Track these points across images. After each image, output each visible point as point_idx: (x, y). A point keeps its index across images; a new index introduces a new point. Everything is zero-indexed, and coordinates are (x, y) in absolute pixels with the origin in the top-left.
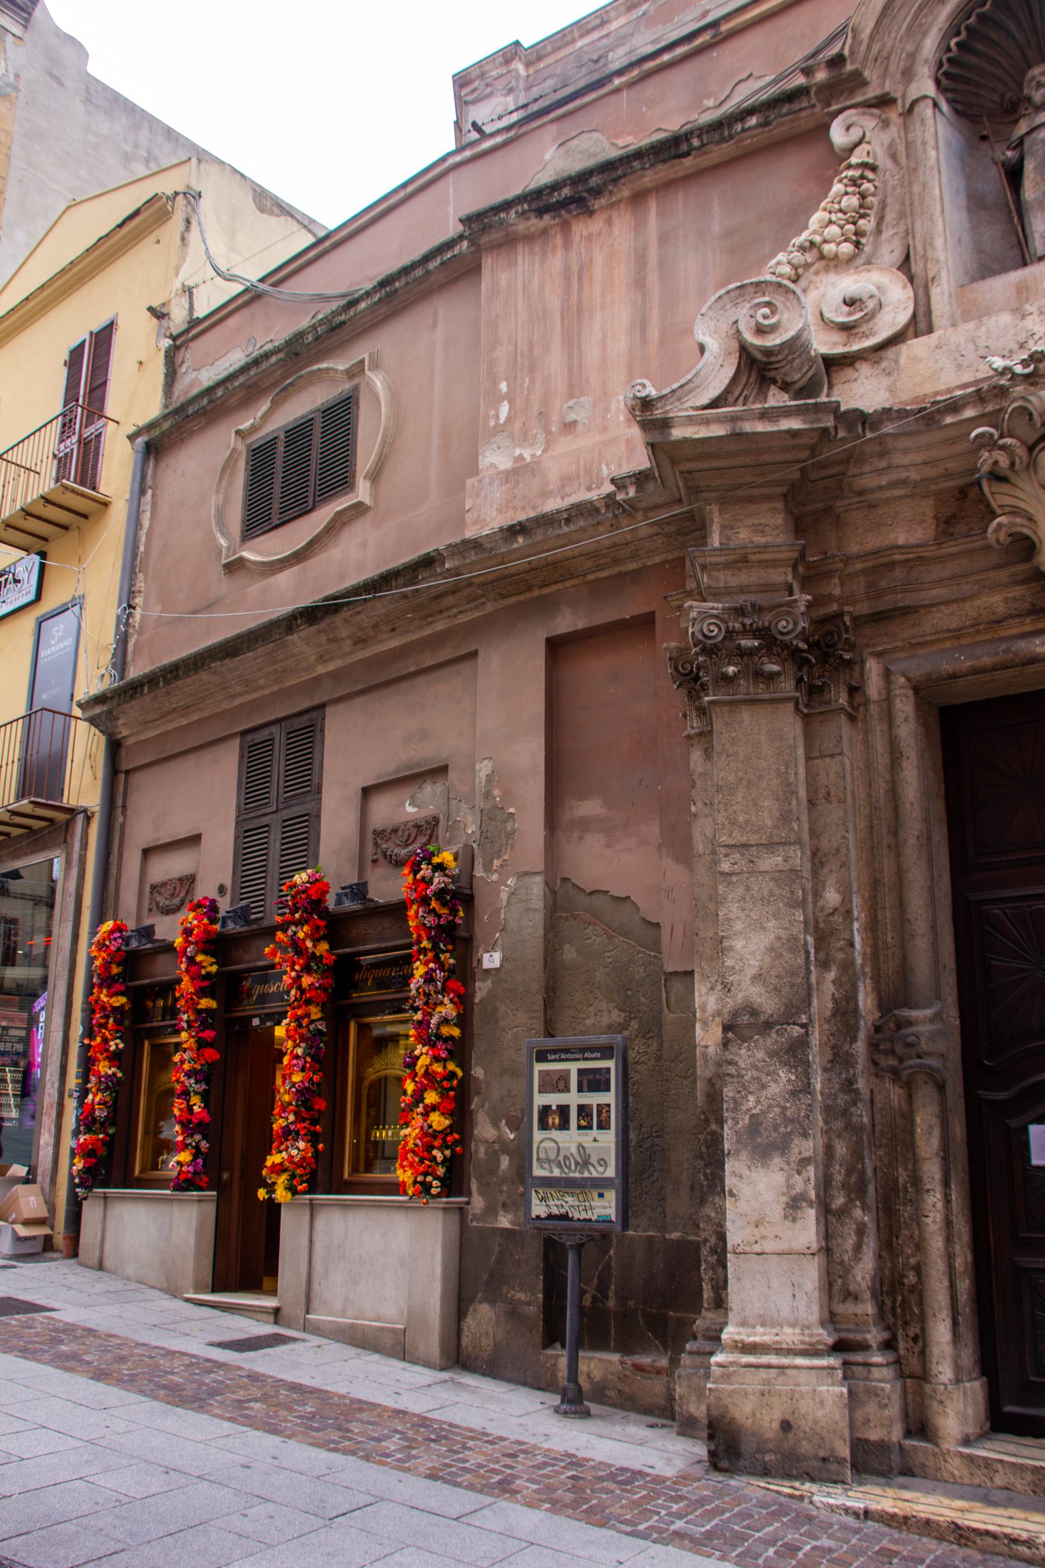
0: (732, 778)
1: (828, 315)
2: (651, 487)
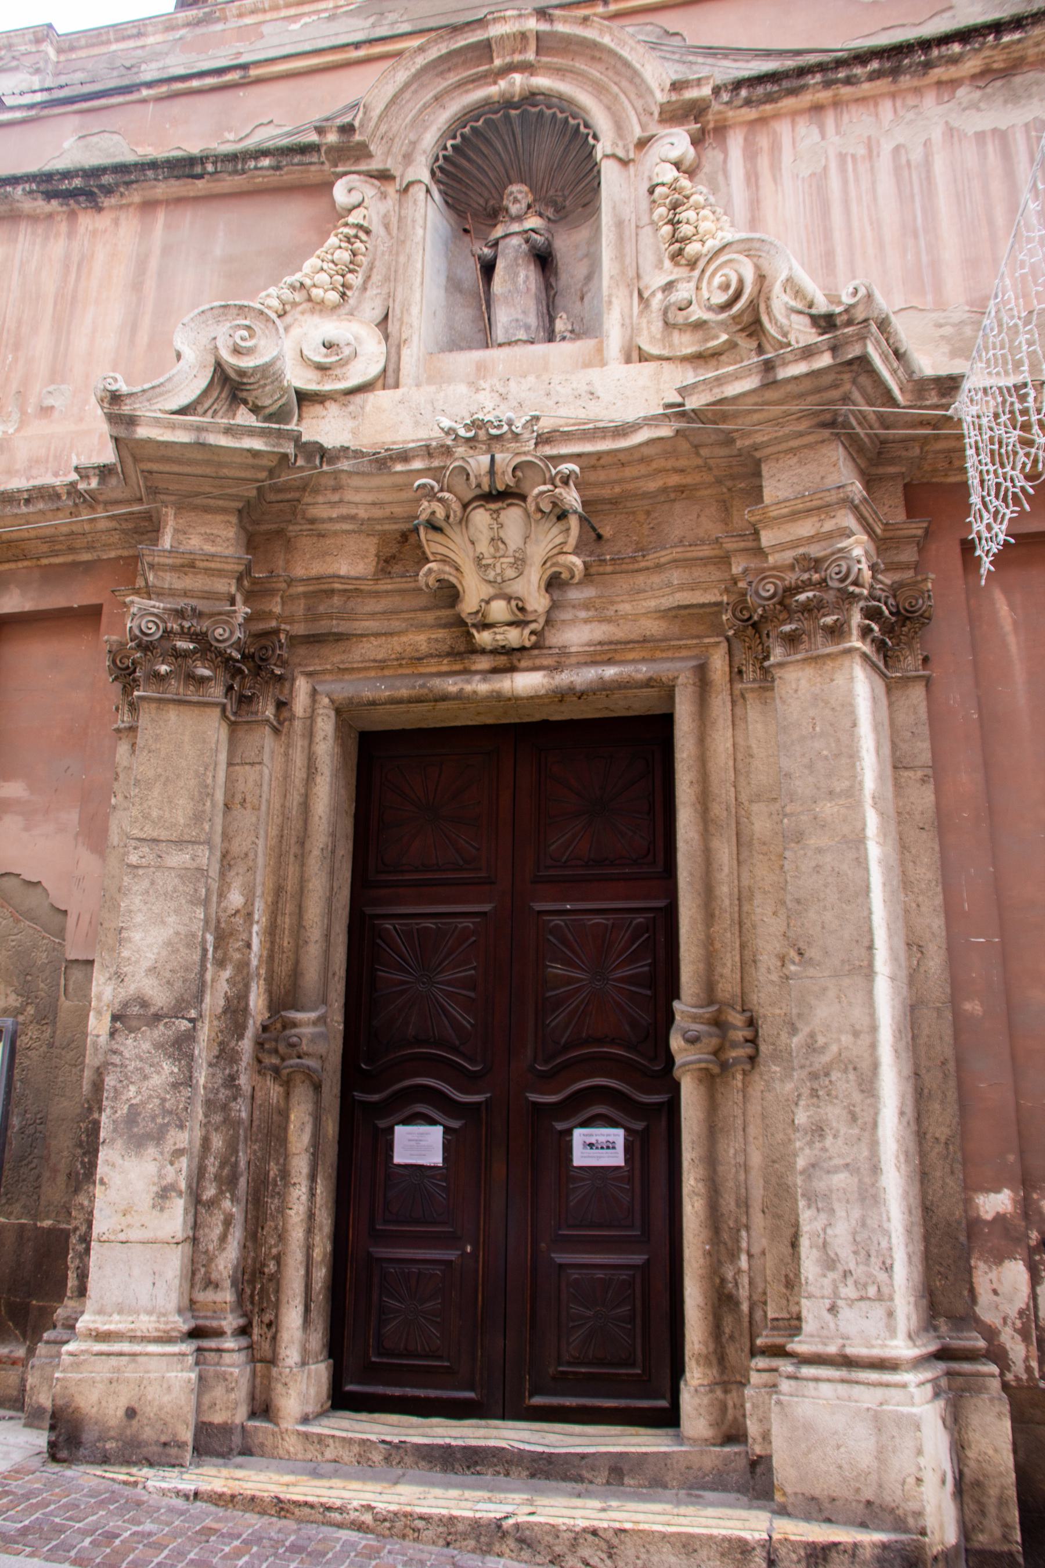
0: (151, 773)
2: (113, 481)
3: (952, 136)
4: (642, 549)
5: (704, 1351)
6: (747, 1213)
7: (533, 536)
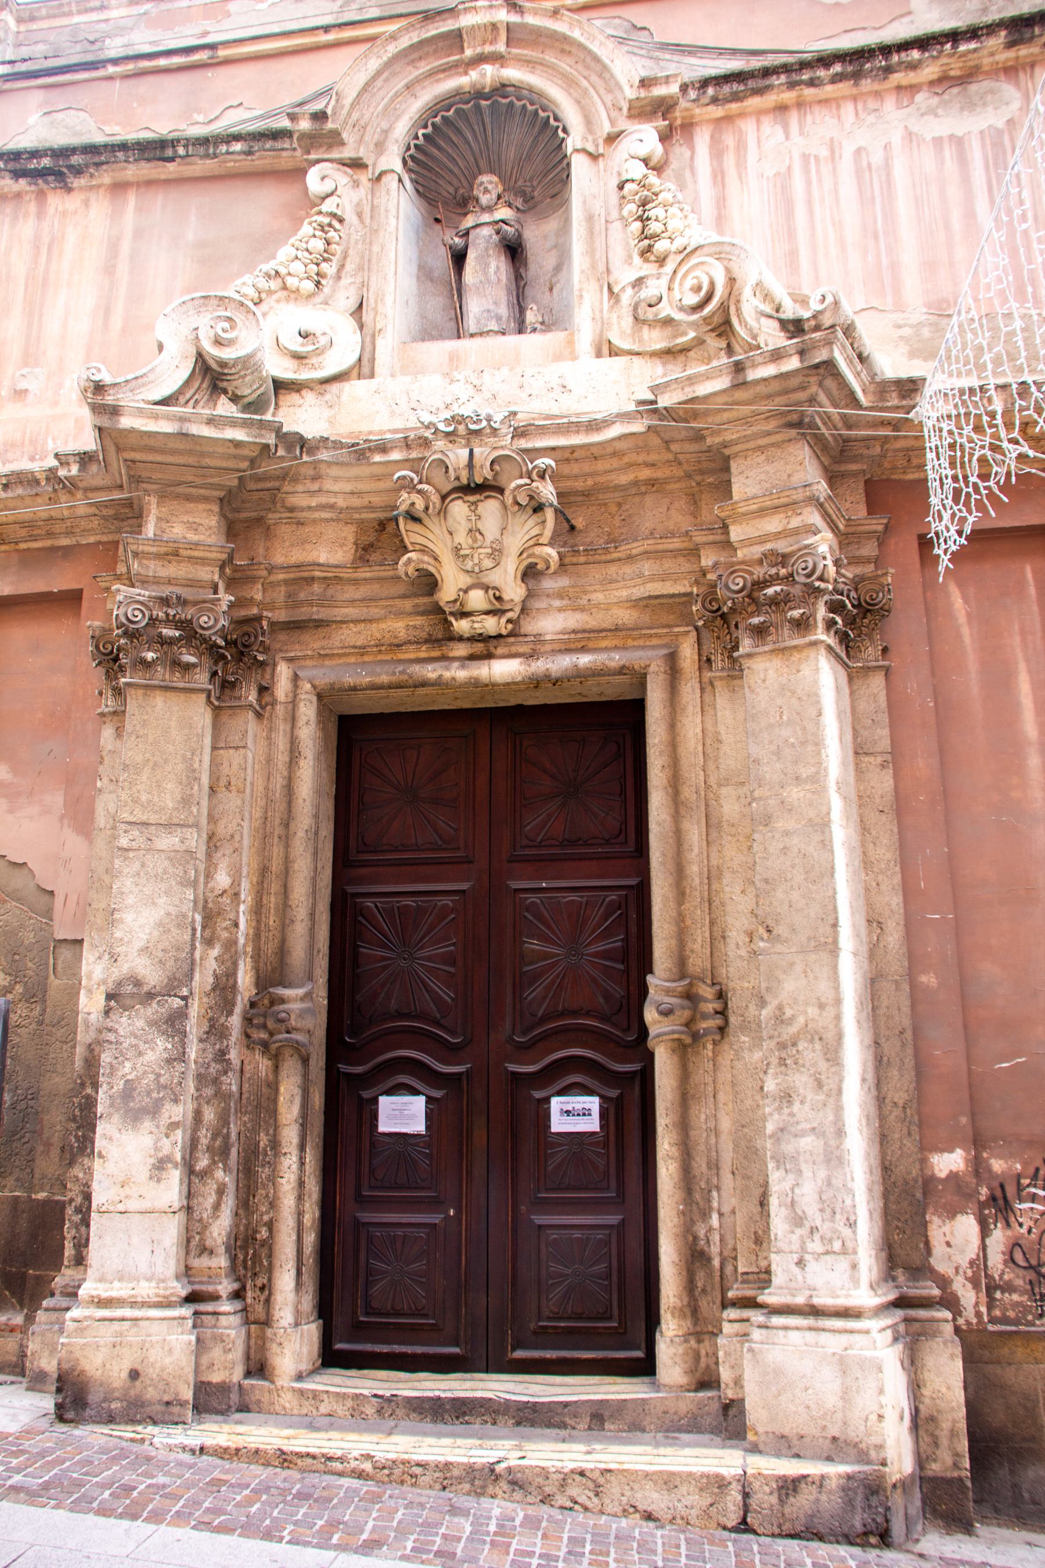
0: (139, 759)
1: (284, 341)
2: (94, 468)
3: (911, 141)
4: (614, 541)
5: (679, 1304)
6: (718, 1174)
7: (509, 527)
